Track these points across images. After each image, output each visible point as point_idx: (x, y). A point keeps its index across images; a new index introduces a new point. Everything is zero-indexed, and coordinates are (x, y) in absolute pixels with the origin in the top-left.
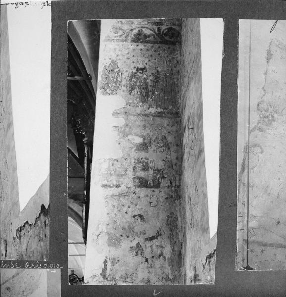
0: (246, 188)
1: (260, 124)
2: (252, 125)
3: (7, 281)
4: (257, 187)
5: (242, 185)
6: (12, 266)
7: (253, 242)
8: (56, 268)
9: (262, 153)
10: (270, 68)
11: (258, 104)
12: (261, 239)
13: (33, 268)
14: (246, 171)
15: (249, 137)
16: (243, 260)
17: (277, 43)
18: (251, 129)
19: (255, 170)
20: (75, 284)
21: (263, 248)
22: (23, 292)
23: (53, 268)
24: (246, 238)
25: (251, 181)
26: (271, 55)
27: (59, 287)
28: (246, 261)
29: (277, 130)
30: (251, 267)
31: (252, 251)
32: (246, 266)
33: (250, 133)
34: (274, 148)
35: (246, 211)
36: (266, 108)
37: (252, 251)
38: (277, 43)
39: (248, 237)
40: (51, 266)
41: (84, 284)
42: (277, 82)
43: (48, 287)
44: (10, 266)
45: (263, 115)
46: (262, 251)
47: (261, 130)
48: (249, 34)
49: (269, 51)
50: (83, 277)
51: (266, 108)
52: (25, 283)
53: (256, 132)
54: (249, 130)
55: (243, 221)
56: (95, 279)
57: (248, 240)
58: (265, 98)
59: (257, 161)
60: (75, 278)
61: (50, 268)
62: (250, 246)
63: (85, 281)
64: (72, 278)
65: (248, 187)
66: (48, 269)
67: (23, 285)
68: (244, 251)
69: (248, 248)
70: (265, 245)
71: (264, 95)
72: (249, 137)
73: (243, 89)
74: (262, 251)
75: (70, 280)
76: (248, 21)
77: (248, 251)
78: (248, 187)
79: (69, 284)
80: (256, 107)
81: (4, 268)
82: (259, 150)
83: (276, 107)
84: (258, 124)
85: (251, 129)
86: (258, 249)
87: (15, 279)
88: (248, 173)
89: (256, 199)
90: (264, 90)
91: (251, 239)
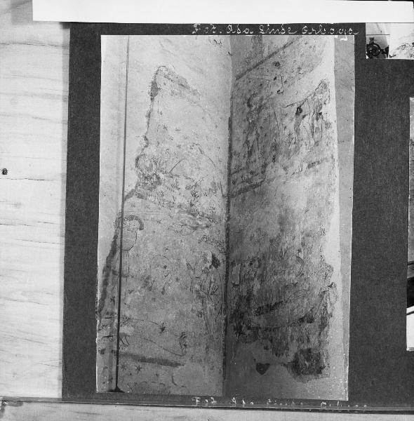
0: (117, 278)
1: (139, 188)
2: (128, 189)
3: (276, 53)
4: (132, 277)
5: (111, 274)
6: (283, 31)
7: (126, 355)
8: (347, 34)
9: (140, 229)
10: (155, 108)
11: (137, 159)
12: (137, 352)
13: (313, 34)
14: (118, 255)
15: (123, 207)
16: (110, 380)
17: (167, 73)
18: (126, 194)
19: (130, 253)
20: (375, 58)
21: (140, 364)
22: (299, 68)
23: (343, 34)
24: (115, 349)
25: (125, 268)
26: (158, 89)
27: (353, 62)
28: (114, 381)
29: (164, 198)
30: (122, 389)
31: (123, 367)
32: (114, 388)
33: (124, 200)
34: (159, 222)
35: (116, 311)
36: (148, 166)
37: (123, 367)
38: (167, 73)
39: (118, 348)
40: (341, 31)
41: (389, 58)
42: (165, 128)
43: (336, 62)
44: (280, 31)
45: (143, 174)
46: (139, 369)
47: (140, 197)
48: (125, 59)
49: (154, 84)
50: (388, 48)
51: (148, 166)
52: (301, 55)
53: (134, 199)
54: (123, 194)
55: (111, 325)
56: (405, 51)
57: (118, 351)
58: (147, 151)
59: (134, 240)
60: (375, 50)
61: (338, 34)
62: (121, 360)
63: (391, 53)
64: (371, 49)
65: (120, 276)
66: (336, 36)
67: (298, 58)
68: (112, 366)
69: (118, 363)
70: (143, 360)
71: (146, 146)
72: (123, 207)
73: (116, 137)
74: (139, 369)
75: (368, 51)
76: (126, 37)
77: (117, 368)
78: (120, 276)
79: (367, 57)
80: (134, 163)
81: (271, 34)
82: (137, 224)
83: (162, 164)
84: (136, 187)
85: (126, 194)
86: (133, 365)
87: (288, 50)
88: (121, 257)
89: (132, 294)
90: (146, 139)
91: (123, 350)
